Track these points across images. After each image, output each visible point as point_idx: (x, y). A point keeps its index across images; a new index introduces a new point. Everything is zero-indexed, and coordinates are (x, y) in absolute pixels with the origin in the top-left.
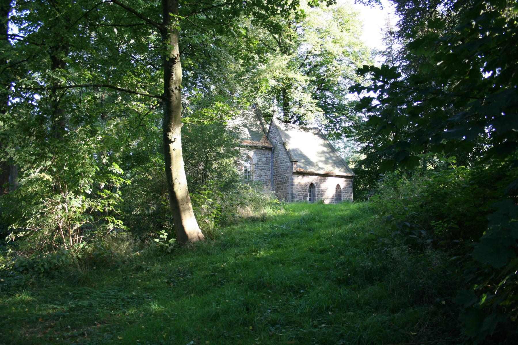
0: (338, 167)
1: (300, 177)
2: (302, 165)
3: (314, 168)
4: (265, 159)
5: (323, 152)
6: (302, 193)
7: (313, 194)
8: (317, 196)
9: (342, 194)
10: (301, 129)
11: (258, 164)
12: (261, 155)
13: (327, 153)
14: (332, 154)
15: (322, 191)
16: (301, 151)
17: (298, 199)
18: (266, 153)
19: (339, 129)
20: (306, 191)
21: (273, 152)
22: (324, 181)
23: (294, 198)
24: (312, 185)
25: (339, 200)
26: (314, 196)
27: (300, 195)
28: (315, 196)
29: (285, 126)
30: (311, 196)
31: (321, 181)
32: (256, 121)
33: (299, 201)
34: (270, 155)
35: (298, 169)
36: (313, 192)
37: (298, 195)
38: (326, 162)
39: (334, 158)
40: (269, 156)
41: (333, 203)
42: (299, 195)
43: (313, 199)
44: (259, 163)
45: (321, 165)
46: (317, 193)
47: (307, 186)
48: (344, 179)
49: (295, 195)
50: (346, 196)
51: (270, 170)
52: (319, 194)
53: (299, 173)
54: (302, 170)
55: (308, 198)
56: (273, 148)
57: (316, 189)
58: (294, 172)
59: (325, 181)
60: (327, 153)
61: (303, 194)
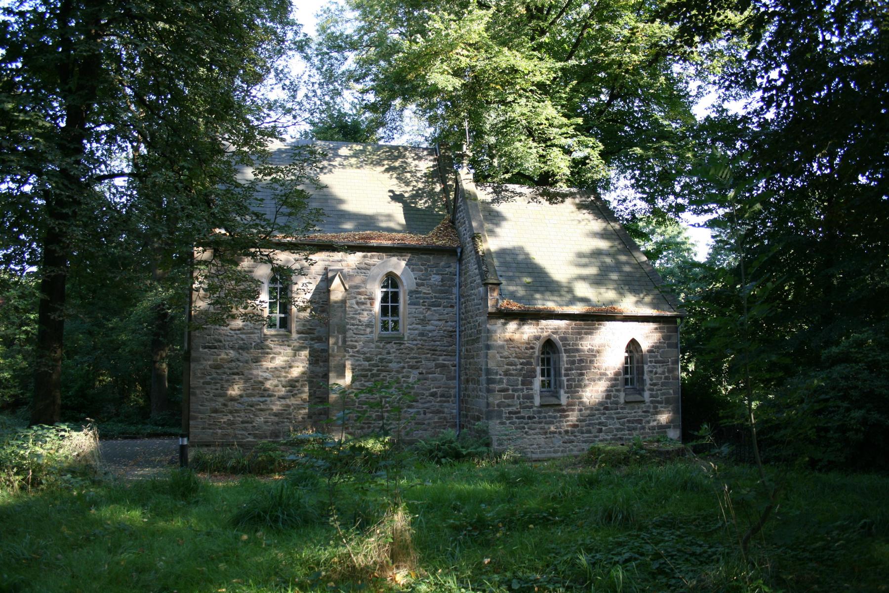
0: (634, 291)
1: (512, 326)
2: (521, 292)
3: (555, 298)
4: (439, 277)
5: (597, 254)
6: (519, 367)
7: (555, 370)
8: (566, 375)
9: (646, 367)
10: (540, 198)
11: (420, 292)
12: (426, 270)
13: (608, 254)
14: (623, 258)
15: (581, 361)
16: (527, 254)
17: (504, 386)
18: (442, 264)
19: (683, 196)
20: (529, 363)
21: (460, 260)
22: (586, 334)
23: (492, 381)
24: (549, 345)
25: (638, 381)
26: (558, 374)
27: (511, 375)
28: (560, 375)
29: (495, 192)
30: (549, 375)
31: (580, 334)
32: (434, 183)
33: (507, 390)
34: (455, 267)
35: (504, 304)
36: (555, 364)
37: (506, 375)
38: (598, 281)
39: (627, 269)
40: (452, 269)
41: (618, 391)
42: (506, 373)
43: (555, 384)
44: (421, 289)
45: (583, 290)
46: (564, 365)
47: (532, 348)
48: (652, 326)
49: (496, 374)
50: (660, 370)
51: (452, 306)
52: (571, 369)
53: (507, 315)
54: (515, 306)
55: (538, 381)
56: (459, 250)
57: (564, 357)
58: (490, 313)
59: (591, 334)
60: (608, 254)
61: (521, 370)
